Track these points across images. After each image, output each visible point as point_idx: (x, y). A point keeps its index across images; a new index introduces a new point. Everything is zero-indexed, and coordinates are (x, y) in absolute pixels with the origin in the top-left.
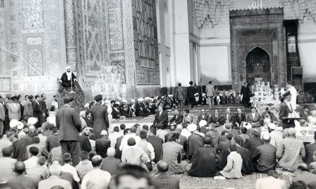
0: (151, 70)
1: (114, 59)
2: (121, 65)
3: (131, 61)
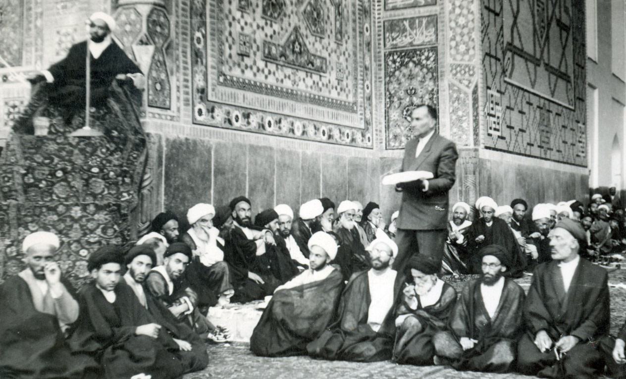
0: (554, 108)
1: (398, 40)
2: (423, 66)
3: (462, 48)
